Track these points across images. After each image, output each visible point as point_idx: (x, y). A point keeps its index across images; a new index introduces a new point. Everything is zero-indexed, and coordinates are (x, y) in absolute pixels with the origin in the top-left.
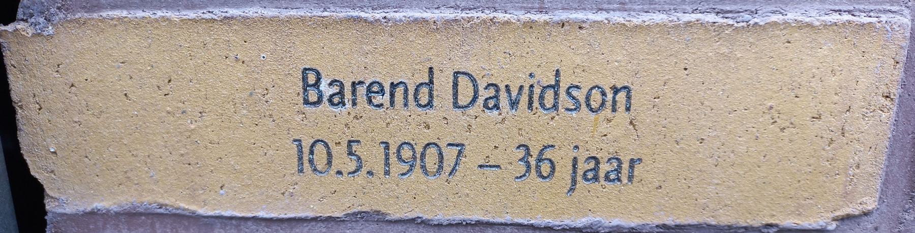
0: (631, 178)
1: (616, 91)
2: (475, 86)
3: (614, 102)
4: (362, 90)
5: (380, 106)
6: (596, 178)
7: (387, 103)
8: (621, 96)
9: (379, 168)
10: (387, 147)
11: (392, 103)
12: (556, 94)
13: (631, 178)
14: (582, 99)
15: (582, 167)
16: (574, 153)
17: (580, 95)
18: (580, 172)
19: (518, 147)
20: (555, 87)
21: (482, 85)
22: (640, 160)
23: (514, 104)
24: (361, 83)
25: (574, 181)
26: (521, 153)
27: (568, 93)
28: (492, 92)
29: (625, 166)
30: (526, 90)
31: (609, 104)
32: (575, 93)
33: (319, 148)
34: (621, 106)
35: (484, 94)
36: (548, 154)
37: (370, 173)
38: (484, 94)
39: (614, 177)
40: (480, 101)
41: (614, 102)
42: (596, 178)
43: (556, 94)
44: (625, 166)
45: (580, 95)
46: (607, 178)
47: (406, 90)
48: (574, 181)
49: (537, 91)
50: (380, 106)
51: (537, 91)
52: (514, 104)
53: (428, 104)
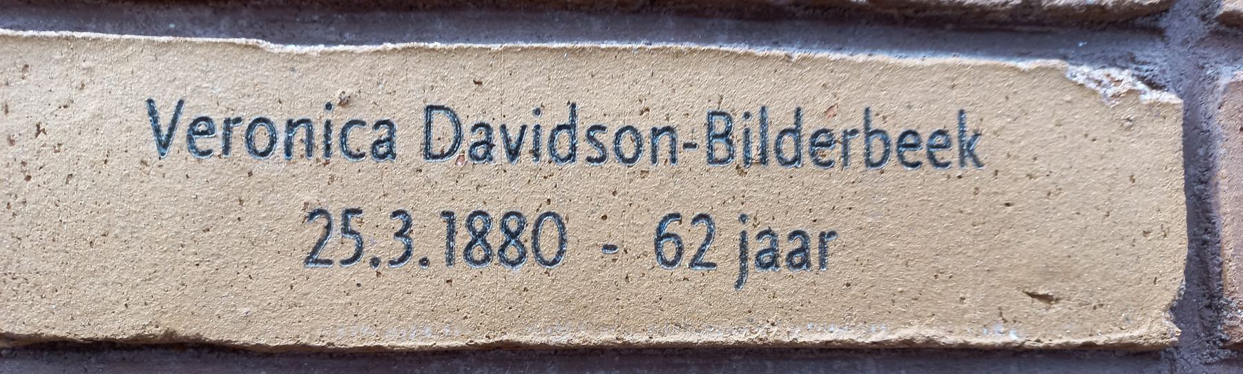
0: (823, 263)
1: (291, 125)
2: (457, 124)
3: (654, 150)
4: (239, 131)
5: (915, 165)
6: (774, 263)
7: (218, 151)
8: (664, 140)
9: (437, 254)
10: (451, 222)
11: (226, 149)
12: (798, 142)
13: (823, 263)
14: (610, 147)
15: (755, 247)
16: (743, 227)
17: (606, 139)
18: (752, 254)
19: (695, 220)
20: (570, 127)
21: (466, 127)
22: (832, 234)
23: (513, 154)
24: (238, 120)
25: (743, 270)
26: (398, 224)
27: (591, 139)
28: (480, 136)
29: (814, 244)
30: (529, 137)
31: (280, 145)
32: (598, 136)
33: (549, 223)
34: (299, 148)
35: (470, 138)
36: (671, 227)
37: (424, 262)
38: (470, 138)
39: (800, 259)
40: (465, 147)
41: (654, 150)
42: (774, 263)
43: (798, 142)
44: (814, 244)
45: (606, 139)
46: (792, 265)
47: (310, 134)
48: (743, 270)
49: (545, 135)
50: (915, 165)
51: (545, 135)
52: (513, 154)
53: (570, 156)
